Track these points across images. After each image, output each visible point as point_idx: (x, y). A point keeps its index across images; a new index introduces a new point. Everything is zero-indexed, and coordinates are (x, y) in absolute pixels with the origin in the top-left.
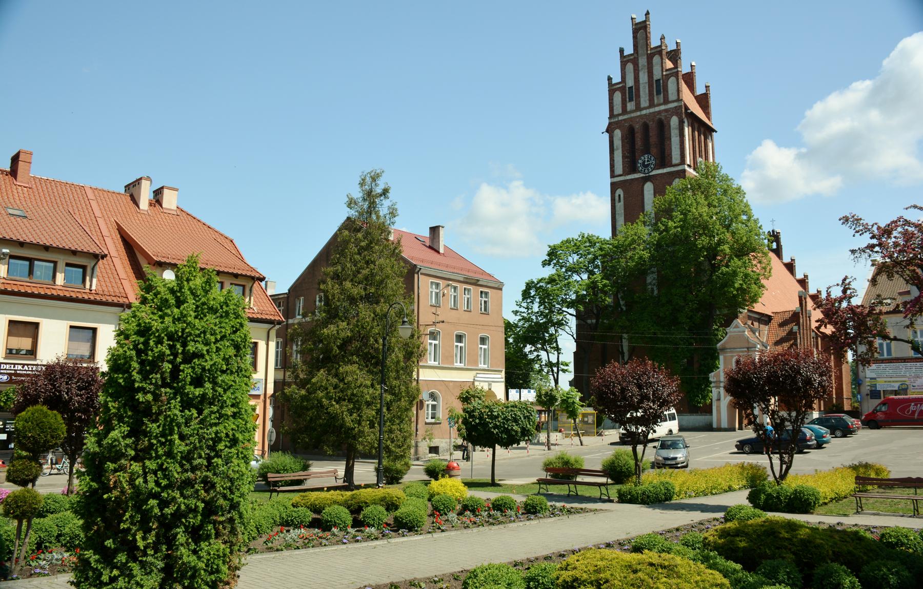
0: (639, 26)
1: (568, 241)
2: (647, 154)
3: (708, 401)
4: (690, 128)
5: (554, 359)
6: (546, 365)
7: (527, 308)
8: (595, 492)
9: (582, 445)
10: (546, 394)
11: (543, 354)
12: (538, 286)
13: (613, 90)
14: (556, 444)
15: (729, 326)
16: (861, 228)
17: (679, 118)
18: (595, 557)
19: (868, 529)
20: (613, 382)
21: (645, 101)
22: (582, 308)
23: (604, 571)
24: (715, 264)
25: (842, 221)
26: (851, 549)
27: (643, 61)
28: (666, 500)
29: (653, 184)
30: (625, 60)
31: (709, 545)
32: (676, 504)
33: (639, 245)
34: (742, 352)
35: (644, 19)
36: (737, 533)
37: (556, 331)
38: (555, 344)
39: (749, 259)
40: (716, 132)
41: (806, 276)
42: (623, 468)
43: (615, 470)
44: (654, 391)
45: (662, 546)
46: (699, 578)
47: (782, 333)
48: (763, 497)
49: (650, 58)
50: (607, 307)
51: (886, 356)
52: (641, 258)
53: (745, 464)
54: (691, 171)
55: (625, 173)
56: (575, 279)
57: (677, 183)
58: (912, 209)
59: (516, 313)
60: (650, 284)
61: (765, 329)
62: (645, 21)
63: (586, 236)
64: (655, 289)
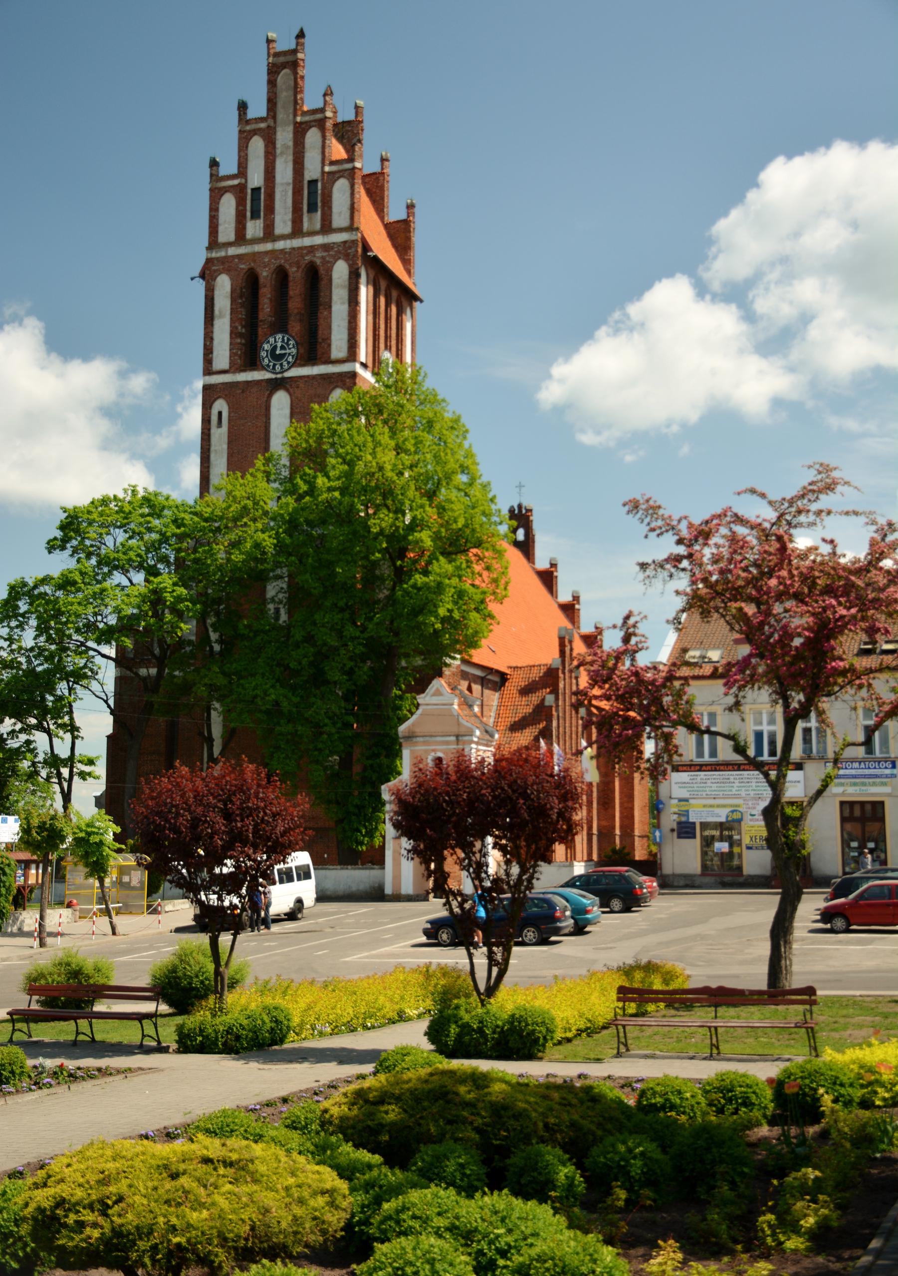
0: (282, 59)
1: (105, 502)
2: (281, 332)
3: (377, 842)
4: (371, 289)
5: (62, 750)
6: (45, 762)
8: (130, 1033)
9: (114, 933)
10: (42, 827)
11: (40, 739)
12: (36, 592)
13: (220, 189)
14: (58, 934)
15: (423, 691)
16: (660, 523)
17: (350, 266)
18: (102, 1156)
19: (627, 1084)
20: (176, 806)
21: (284, 222)
22: (128, 643)
23: (117, 1180)
24: (401, 567)
25: (627, 508)
26: (576, 1117)
27: (284, 137)
28: (274, 1042)
29: (290, 395)
30: (248, 128)
31: (331, 1123)
32: (294, 1050)
33: (254, 520)
34: (447, 743)
35: (293, 46)
36: (384, 1098)
37: (70, 689)
38: (66, 719)
39: (467, 561)
40: (421, 301)
41: (576, 598)
42: (195, 980)
43: (178, 984)
44: (256, 826)
45: (246, 1131)
46: (291, 1181)
47: (525, 706)
48: (453, 1030)
49: (300, 131)
50: (182, 643)
51: (707, 758)
52: (257, 545)
53: (433, 967)
54: (367, 375)
55: (234, 368)
56: (116, 582)
57: (338, 395)
58: (748, 496)
60: (273, 600)
61: (493, 698)
62: (294, 52)
63: (141, 493)
64: (283, 612)
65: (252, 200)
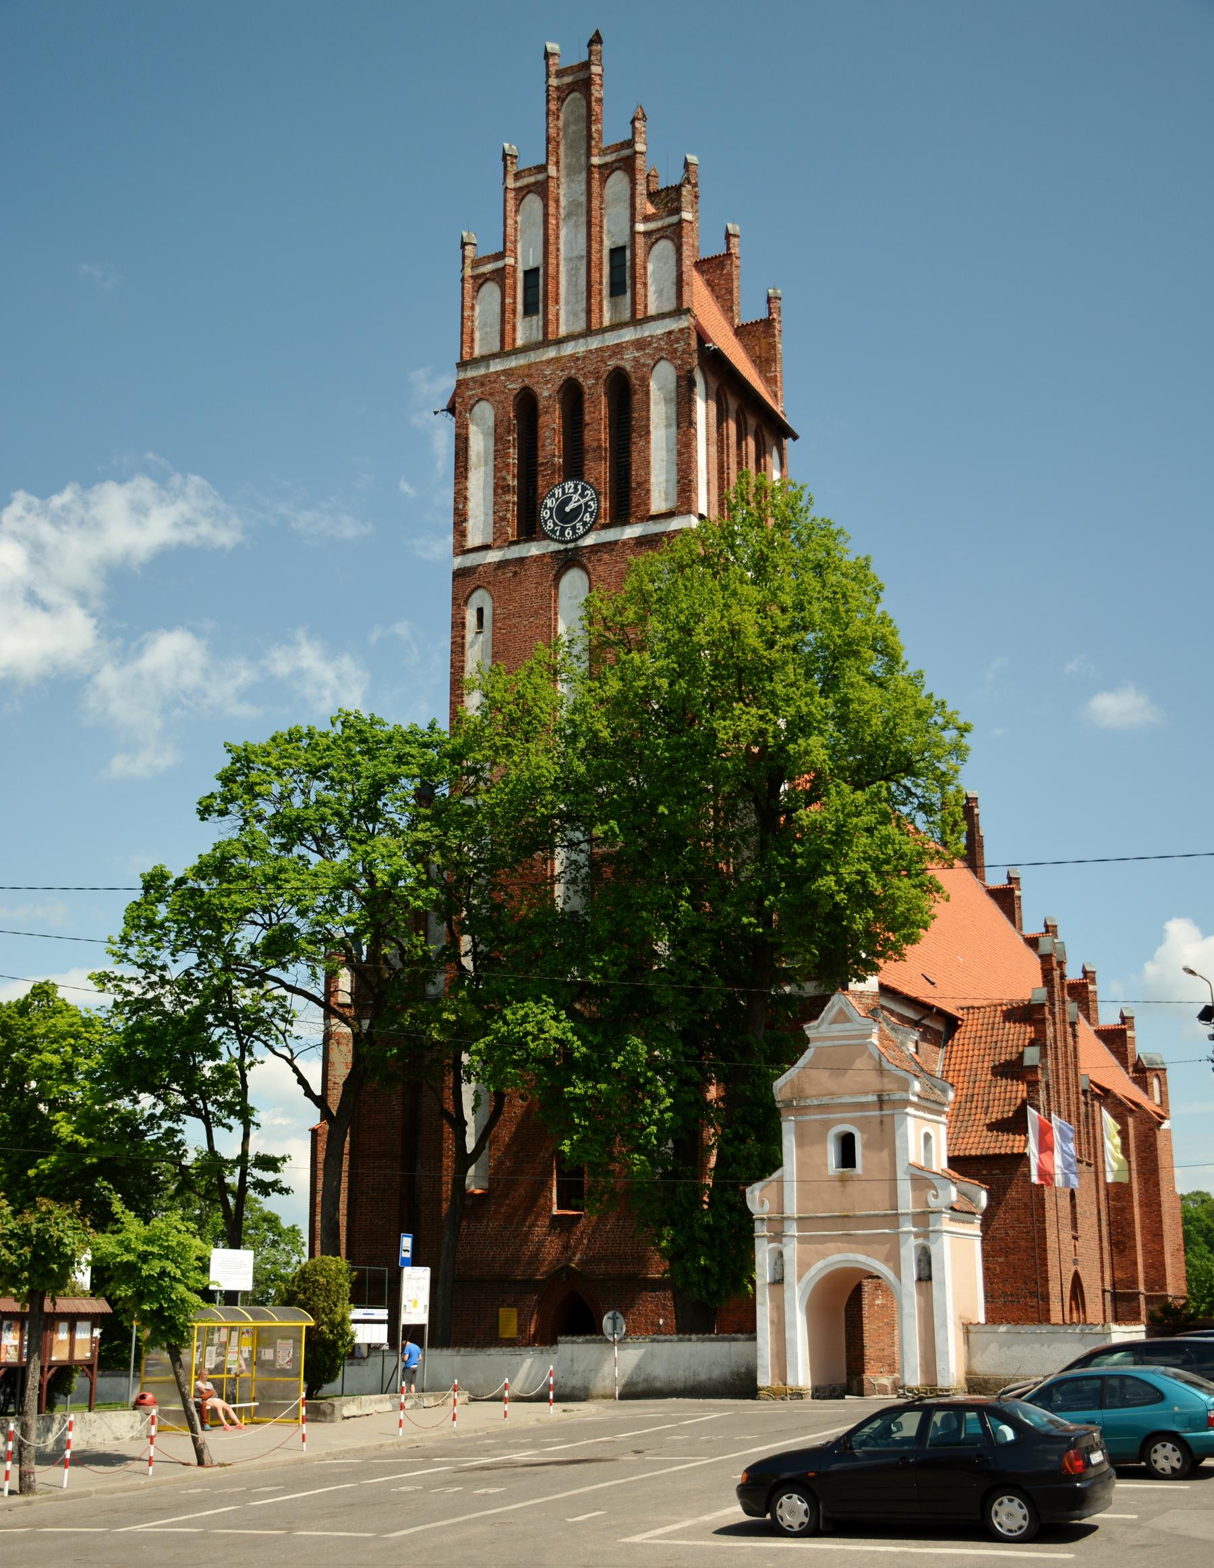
1: (293, 737)
4: (713, 406)
5: (228, 1145)
7: (148, 967)
9: (201, 1463)
11: (192, 1132)
15: (816, 1018)
34: (862, 1106)
40: (795, 437)
59: (102, 979)
62: (586, 65)
65: (526, 288)
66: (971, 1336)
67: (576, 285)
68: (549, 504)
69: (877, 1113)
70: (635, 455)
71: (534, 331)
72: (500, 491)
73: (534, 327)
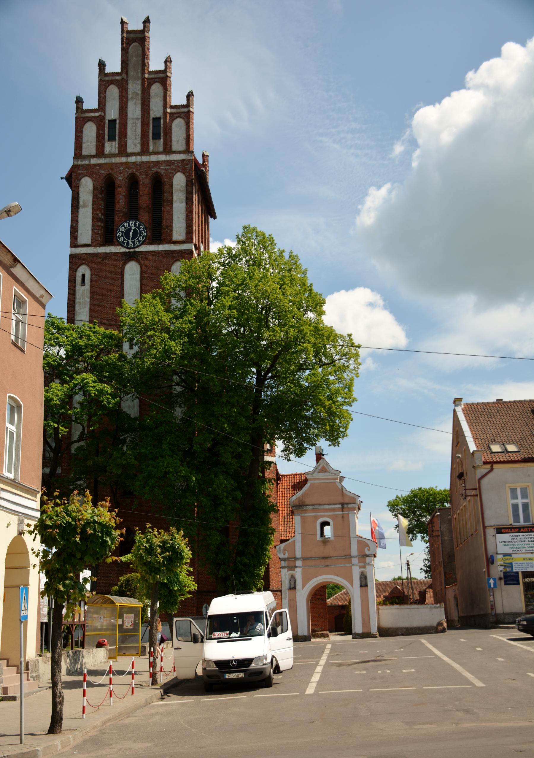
66: (380, 611)
67: (135, 131)
68: (121, 229)
69: (341, 513)
70: (165, 213)
71: (114, 149)
72: (95, 220)
73: (113, 147)
